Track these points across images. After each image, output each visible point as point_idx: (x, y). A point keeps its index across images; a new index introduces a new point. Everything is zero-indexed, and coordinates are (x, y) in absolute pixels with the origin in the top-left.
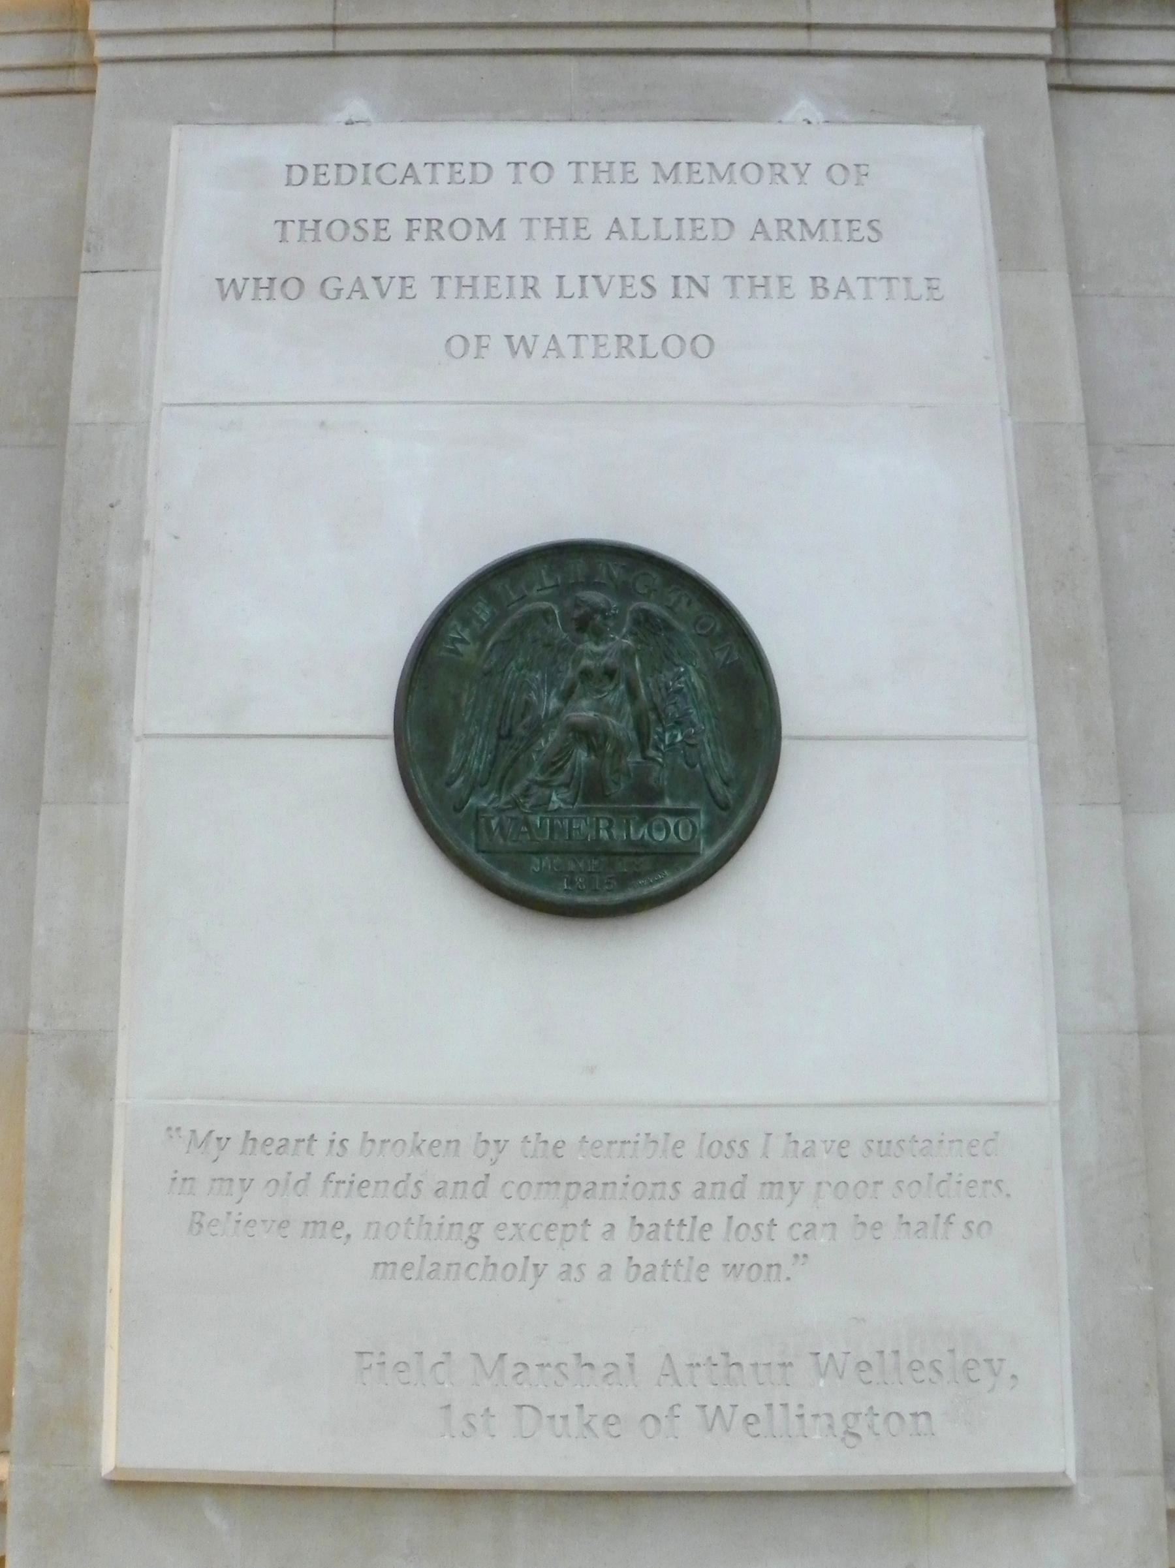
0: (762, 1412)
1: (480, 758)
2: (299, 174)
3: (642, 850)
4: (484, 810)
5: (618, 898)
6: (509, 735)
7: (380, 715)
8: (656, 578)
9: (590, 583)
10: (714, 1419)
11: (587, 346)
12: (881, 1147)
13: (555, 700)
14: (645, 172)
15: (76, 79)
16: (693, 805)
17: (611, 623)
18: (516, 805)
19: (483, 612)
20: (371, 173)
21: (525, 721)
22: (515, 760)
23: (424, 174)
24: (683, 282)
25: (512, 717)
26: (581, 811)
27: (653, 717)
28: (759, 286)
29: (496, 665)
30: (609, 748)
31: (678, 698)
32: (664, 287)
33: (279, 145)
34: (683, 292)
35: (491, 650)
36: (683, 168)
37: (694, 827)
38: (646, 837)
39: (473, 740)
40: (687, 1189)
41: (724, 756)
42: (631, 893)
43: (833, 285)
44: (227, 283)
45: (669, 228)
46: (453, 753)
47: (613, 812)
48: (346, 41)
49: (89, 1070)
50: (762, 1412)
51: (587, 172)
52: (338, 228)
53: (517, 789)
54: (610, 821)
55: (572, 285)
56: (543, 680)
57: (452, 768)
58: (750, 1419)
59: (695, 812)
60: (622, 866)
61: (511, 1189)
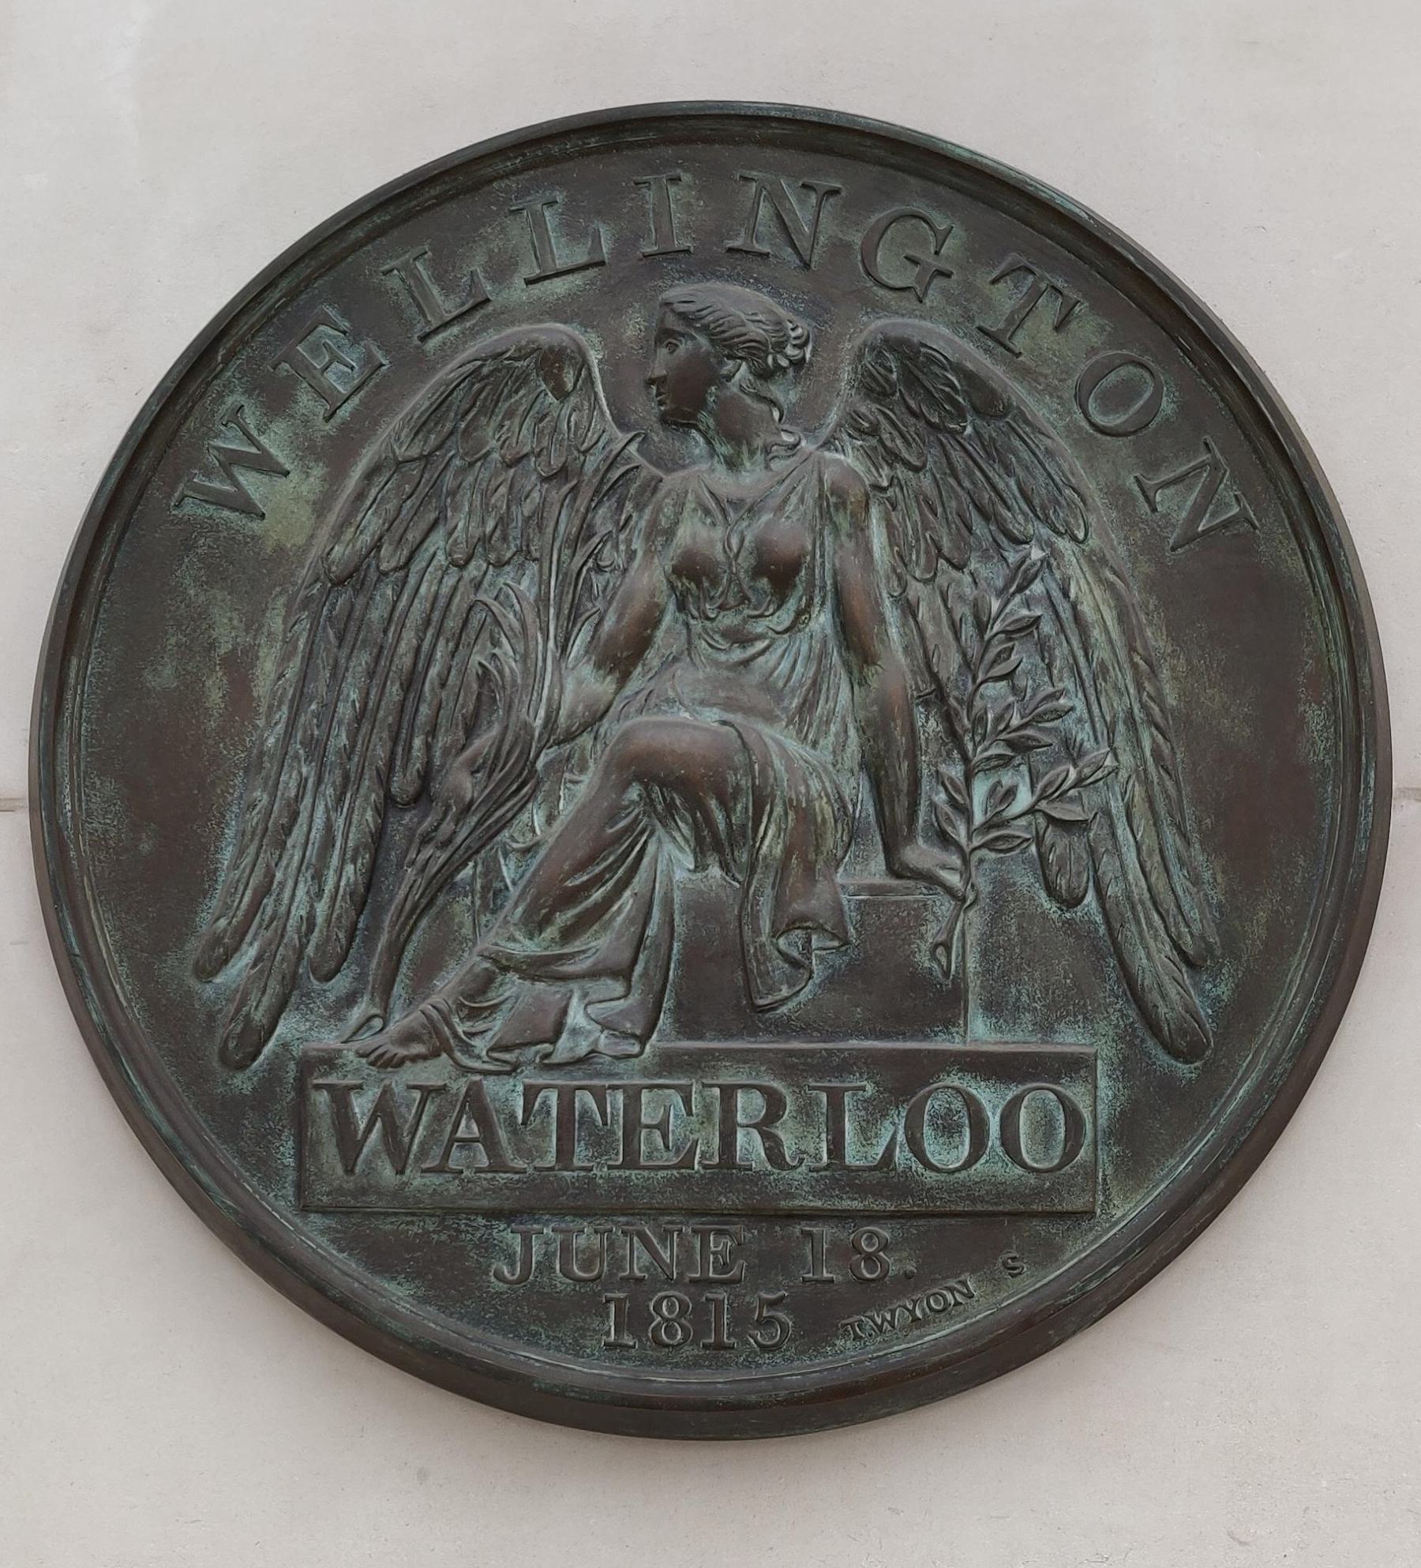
3: (892, 1193)
5: (802, 1371)
16: (1070, 1040)
22: (443, 882)
53: (447, 984)
57: (212, 918)
59: (1075, 1066)
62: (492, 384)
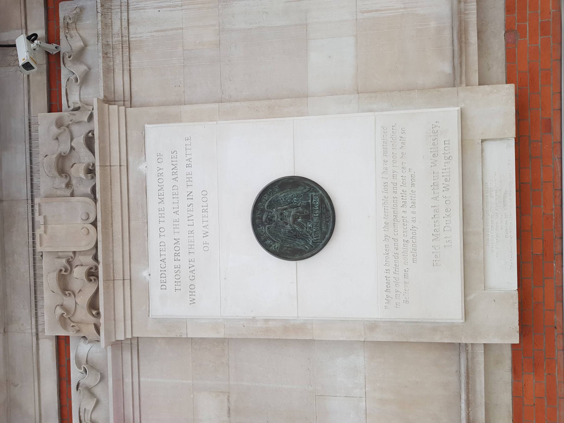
0: (444, 178)
2: (163, 286)
7: (292, 263)
9: (261, 218)
10: (446, 188)
11: (205, 219)
12: (385, 153)
14: (161, 206)
15: (135, 342)
16: (310, 195)
20: (163, 270)
23: (163, 257)
24: (189, 197)
28: (189, 180)
32: (190, 202)
33: (155, 292)
34: (191, 197)
36: (160, 197)
40: (395, 195)
42: (330, 209)
43: (189, 163)
44: (191, 302)
45: (175, 200)
47: (312, 213)
48: (127, 277)
49: (373, 326)
50: (444, 178)
51: (162, 219)
52: (177, 277)
55: (191, 223)
58: (446, 180)
60: (324, 211)
61: (396, 233)
62: (270, 232)
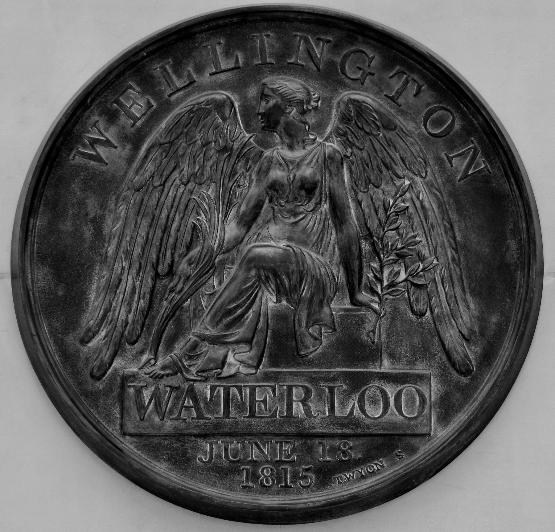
1: (130, 305)
4: (134, 377)
6: (171, 272)
8: (374, 57)
9: (282, 66)
13: (233, 224)
16: (420, 369)
17: (311, 119)
18: (176, 368)
19: (136, 103)
21: (192, 253)
25: (174, 247)
26: (267, 377)
27: (366, 247)
29: (152, 176)
30: (306, 292)
31: (401, 221)
35: (146, 157)
37: (422, 396)
38: (357, 412)
39: (120, 281)
41: (465, 301)
46: (92, 296)
47: (314, 379)
53: (179, 348)
54: (308, 391)
56: (217, 198)
57: (89, 319)
59: (420, 378)
60: (321, 454)
62: (198, 115)
